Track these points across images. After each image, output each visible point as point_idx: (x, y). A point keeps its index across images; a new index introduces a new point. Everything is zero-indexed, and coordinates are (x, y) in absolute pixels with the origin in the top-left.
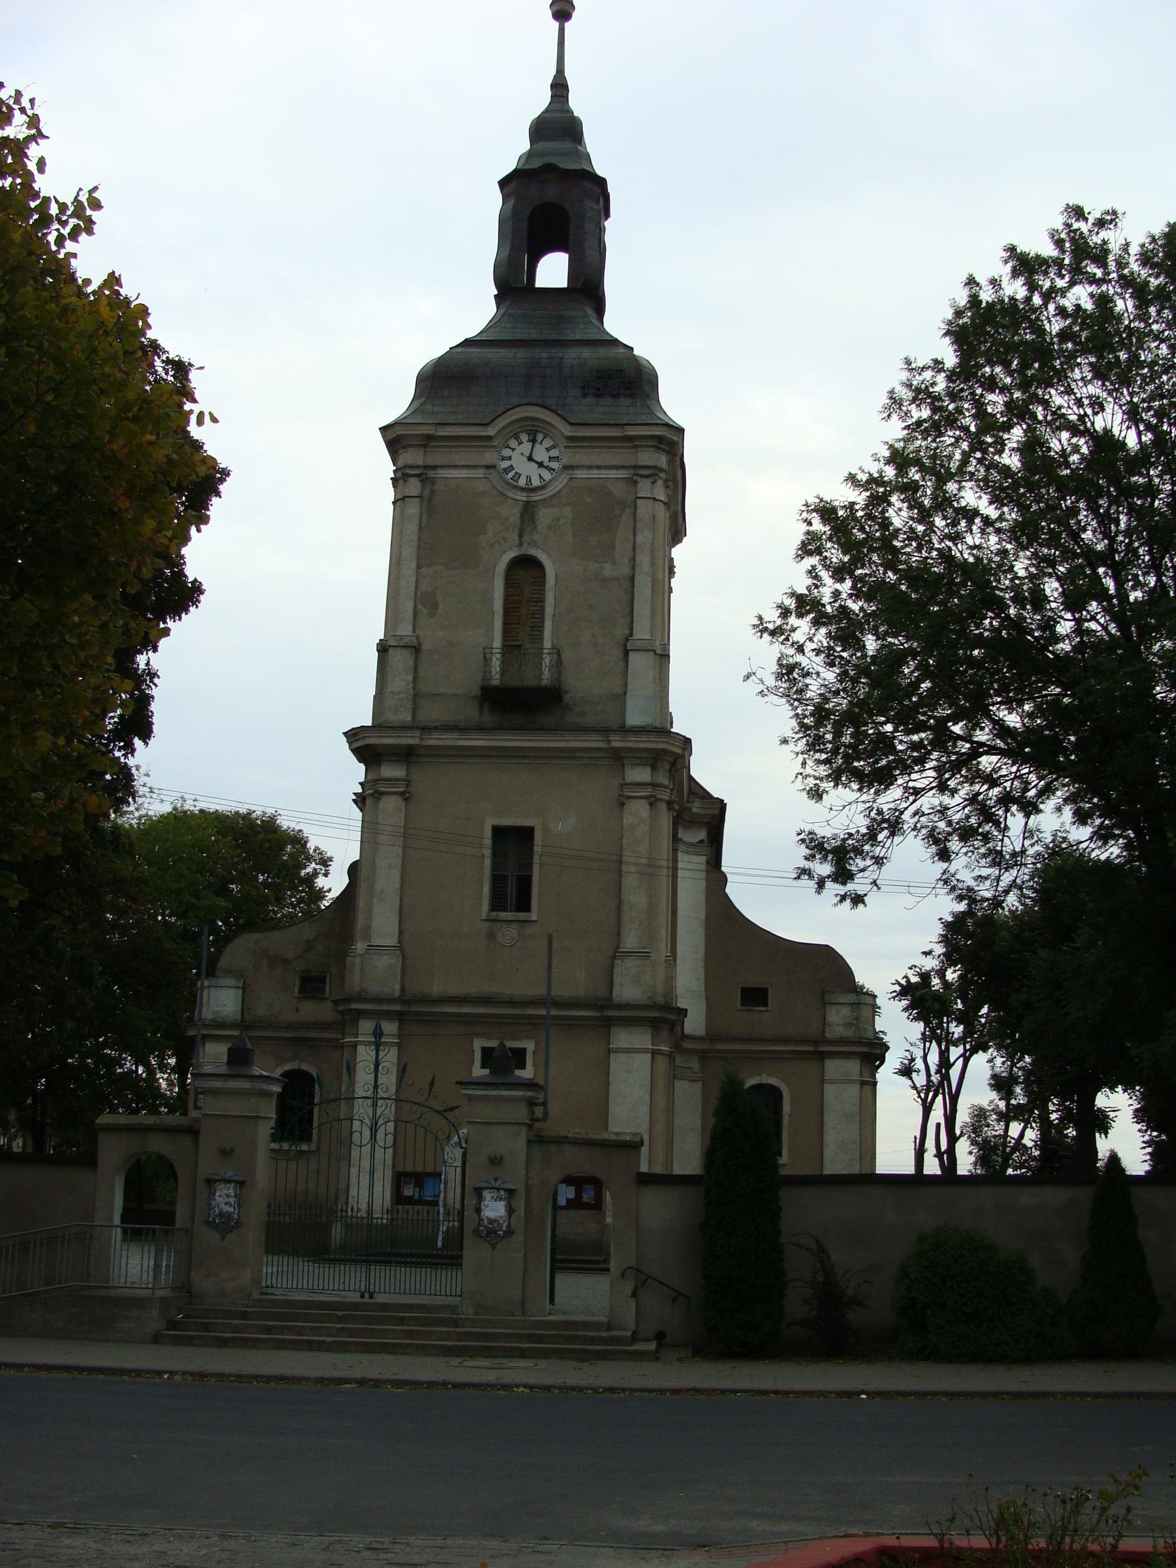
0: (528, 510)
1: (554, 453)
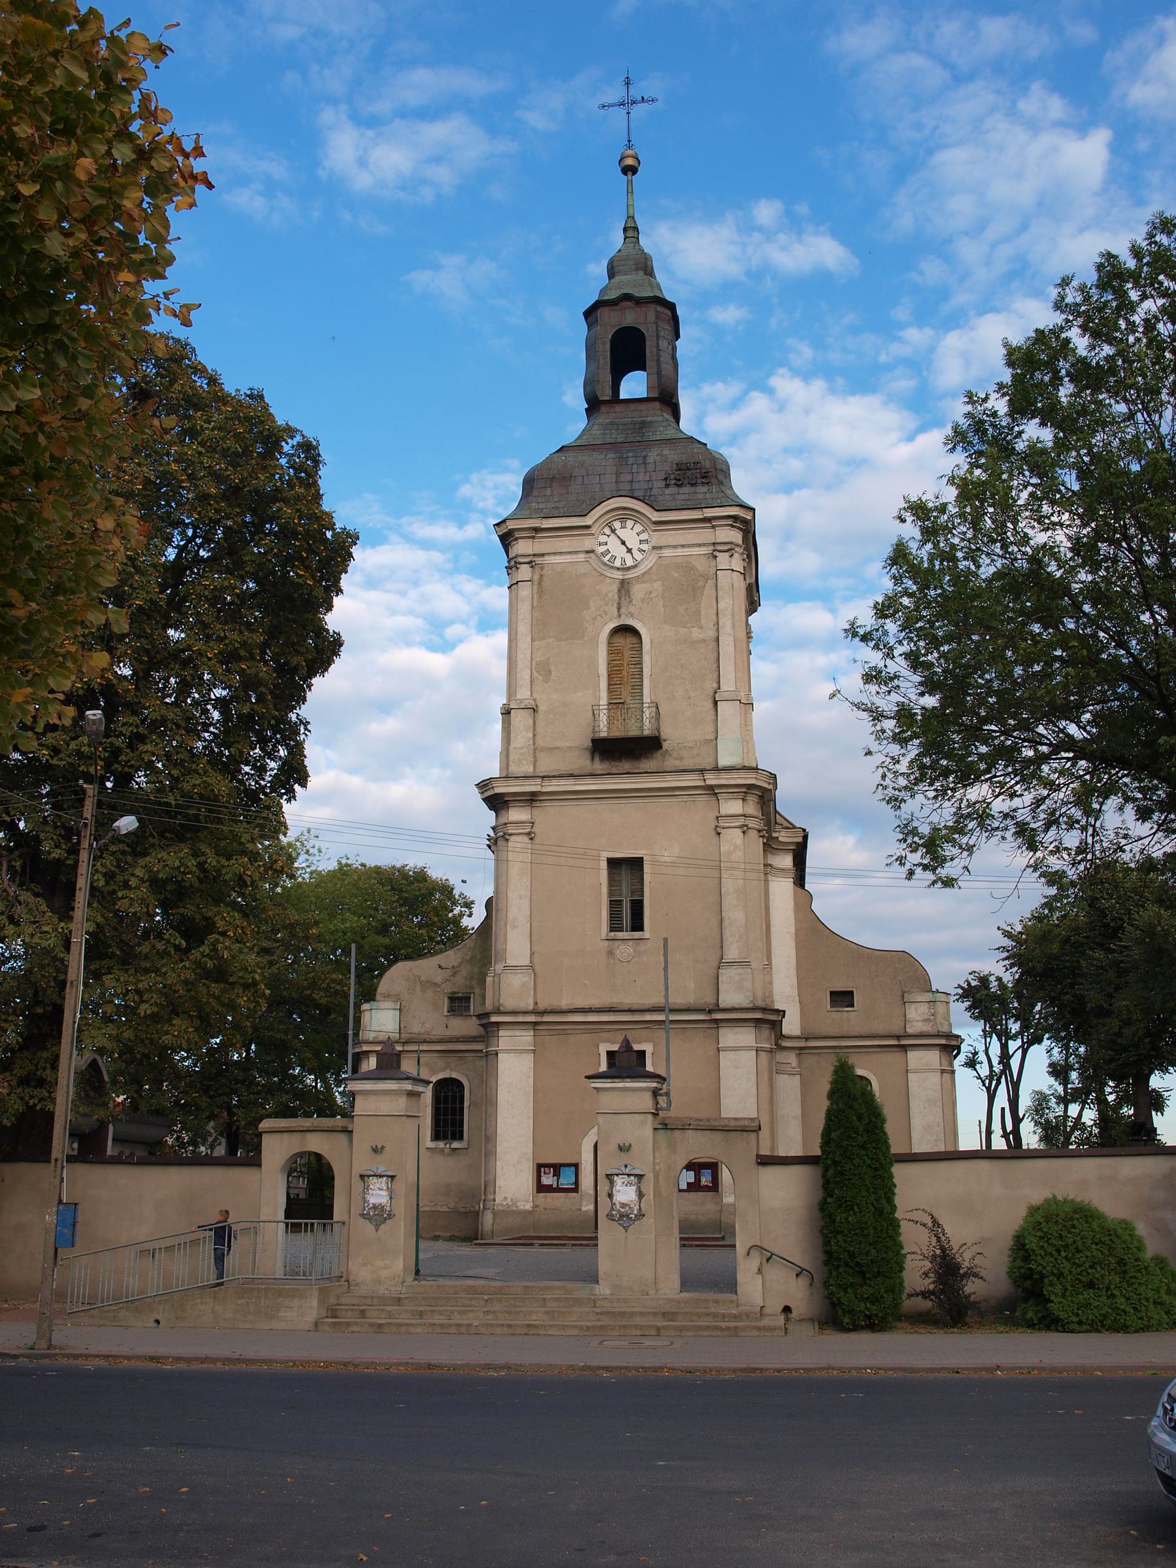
0: (624, 586)
1: (644, 536)
